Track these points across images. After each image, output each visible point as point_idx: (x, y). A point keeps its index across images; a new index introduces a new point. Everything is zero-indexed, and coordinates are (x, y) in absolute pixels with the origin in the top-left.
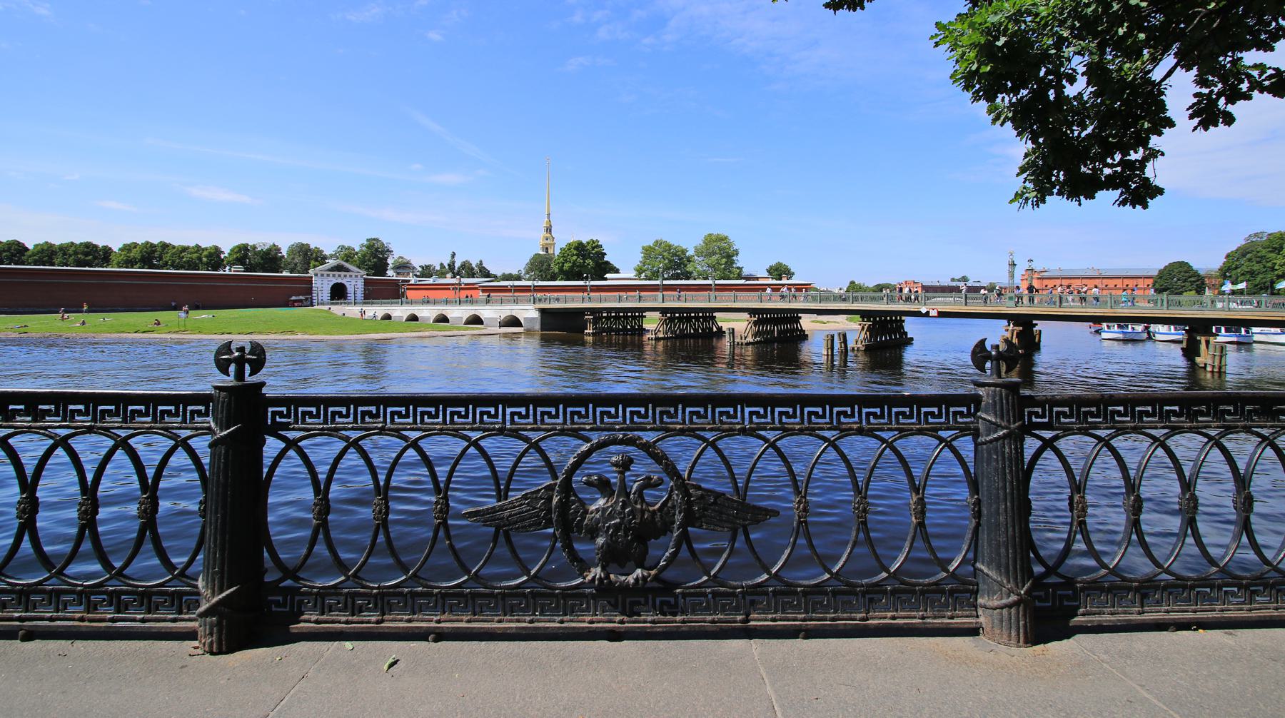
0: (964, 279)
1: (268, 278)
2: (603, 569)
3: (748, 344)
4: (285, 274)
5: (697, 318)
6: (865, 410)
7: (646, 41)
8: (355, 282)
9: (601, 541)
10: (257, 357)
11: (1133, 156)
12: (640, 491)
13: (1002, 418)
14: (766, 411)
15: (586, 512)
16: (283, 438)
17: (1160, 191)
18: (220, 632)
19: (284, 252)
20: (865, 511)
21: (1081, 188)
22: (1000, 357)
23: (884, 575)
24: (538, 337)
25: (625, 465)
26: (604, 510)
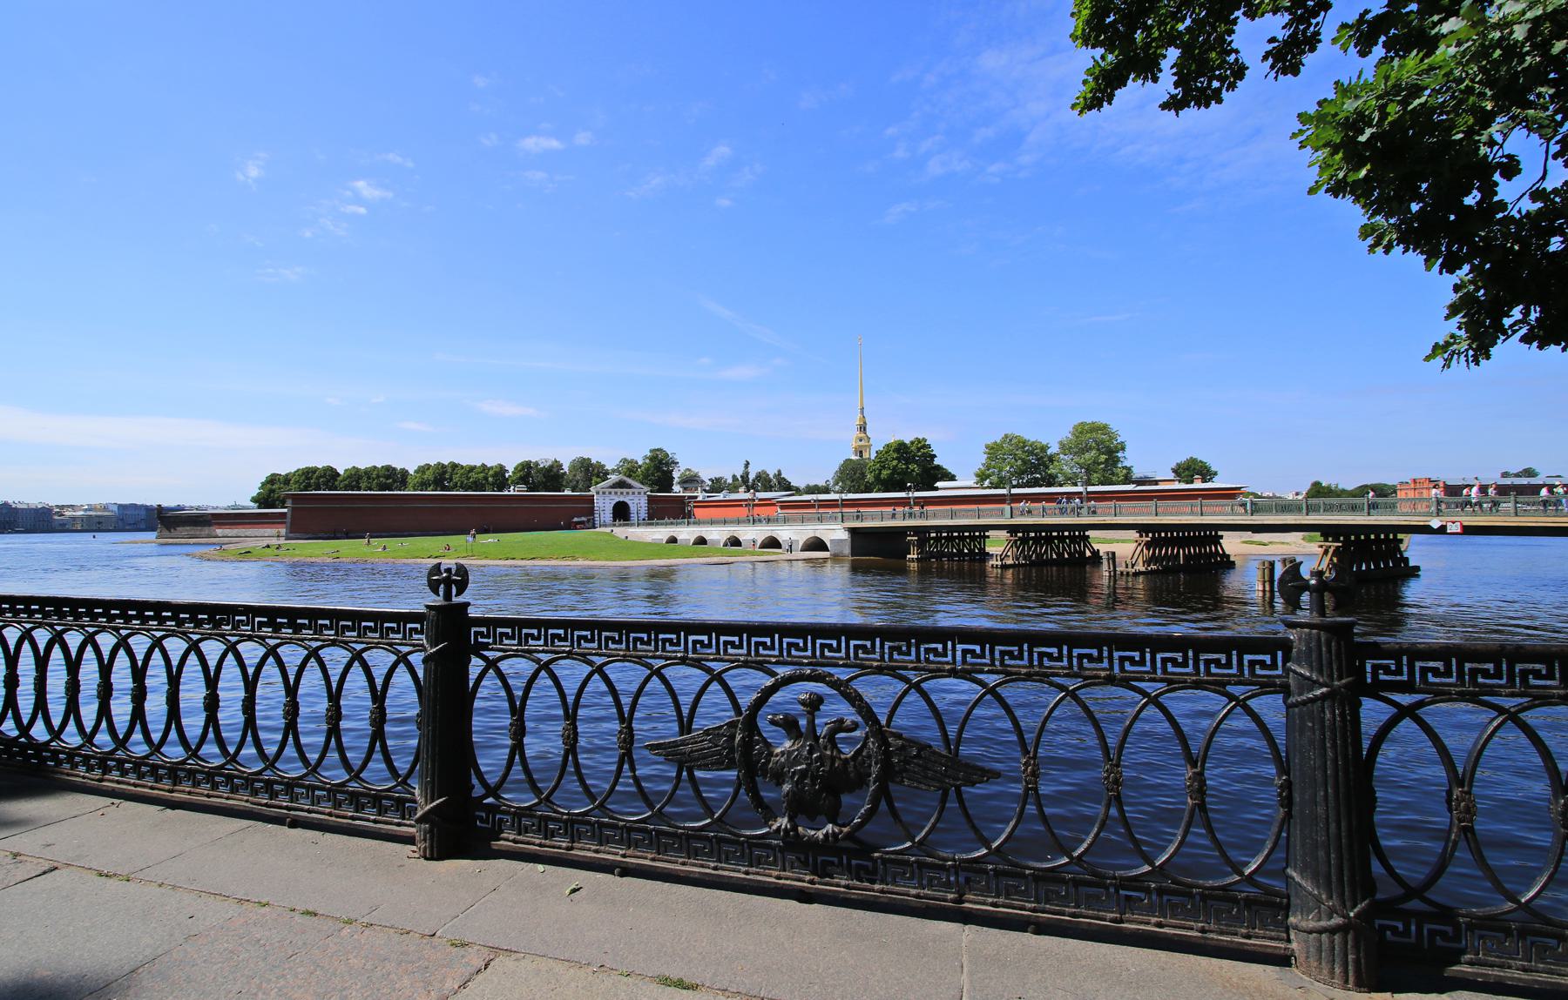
1: (546, 499)
2: (790, 820)
3: (1137, 574)
4: (567, 492)
6: (1116, 655)
7: (993, 168)
8: (638, 501)
9: (786, 787)
10: (459, 579)
13: (1320, 672)
14: (983, 650)
15: (771, 754)
16: (485, 658)
18: (432, 839)
19: (566, 468)
20: (1116, 782)
22: (1322, 587)
23: (1147, 868)
24: (847, 566)
25: (814, 703)
26: (790, 753)
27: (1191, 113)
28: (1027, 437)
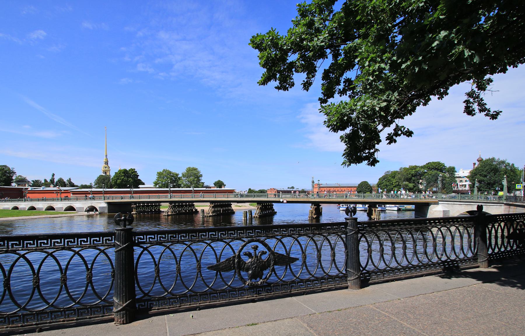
0: (293, 188)
3: (210, 216)
5: (186, 206)
7: (162, 74)
9: (250, 272)
11: (372, 151)
12: (261, 255)
17: (378, 161)
21: (359, 160)
25: (256, 248)
26: (251, 262)
27: (281, 91)
28: (171, 170)
